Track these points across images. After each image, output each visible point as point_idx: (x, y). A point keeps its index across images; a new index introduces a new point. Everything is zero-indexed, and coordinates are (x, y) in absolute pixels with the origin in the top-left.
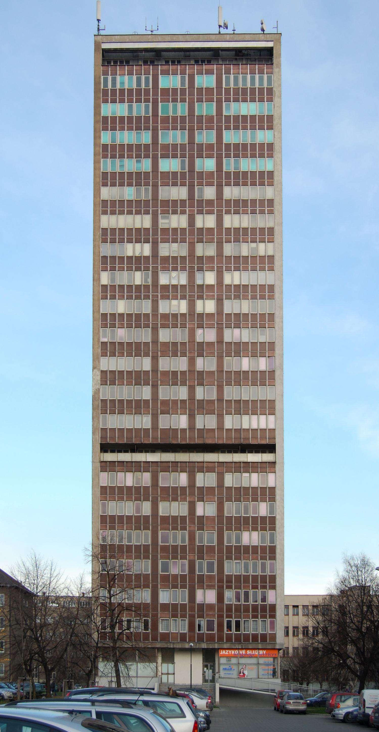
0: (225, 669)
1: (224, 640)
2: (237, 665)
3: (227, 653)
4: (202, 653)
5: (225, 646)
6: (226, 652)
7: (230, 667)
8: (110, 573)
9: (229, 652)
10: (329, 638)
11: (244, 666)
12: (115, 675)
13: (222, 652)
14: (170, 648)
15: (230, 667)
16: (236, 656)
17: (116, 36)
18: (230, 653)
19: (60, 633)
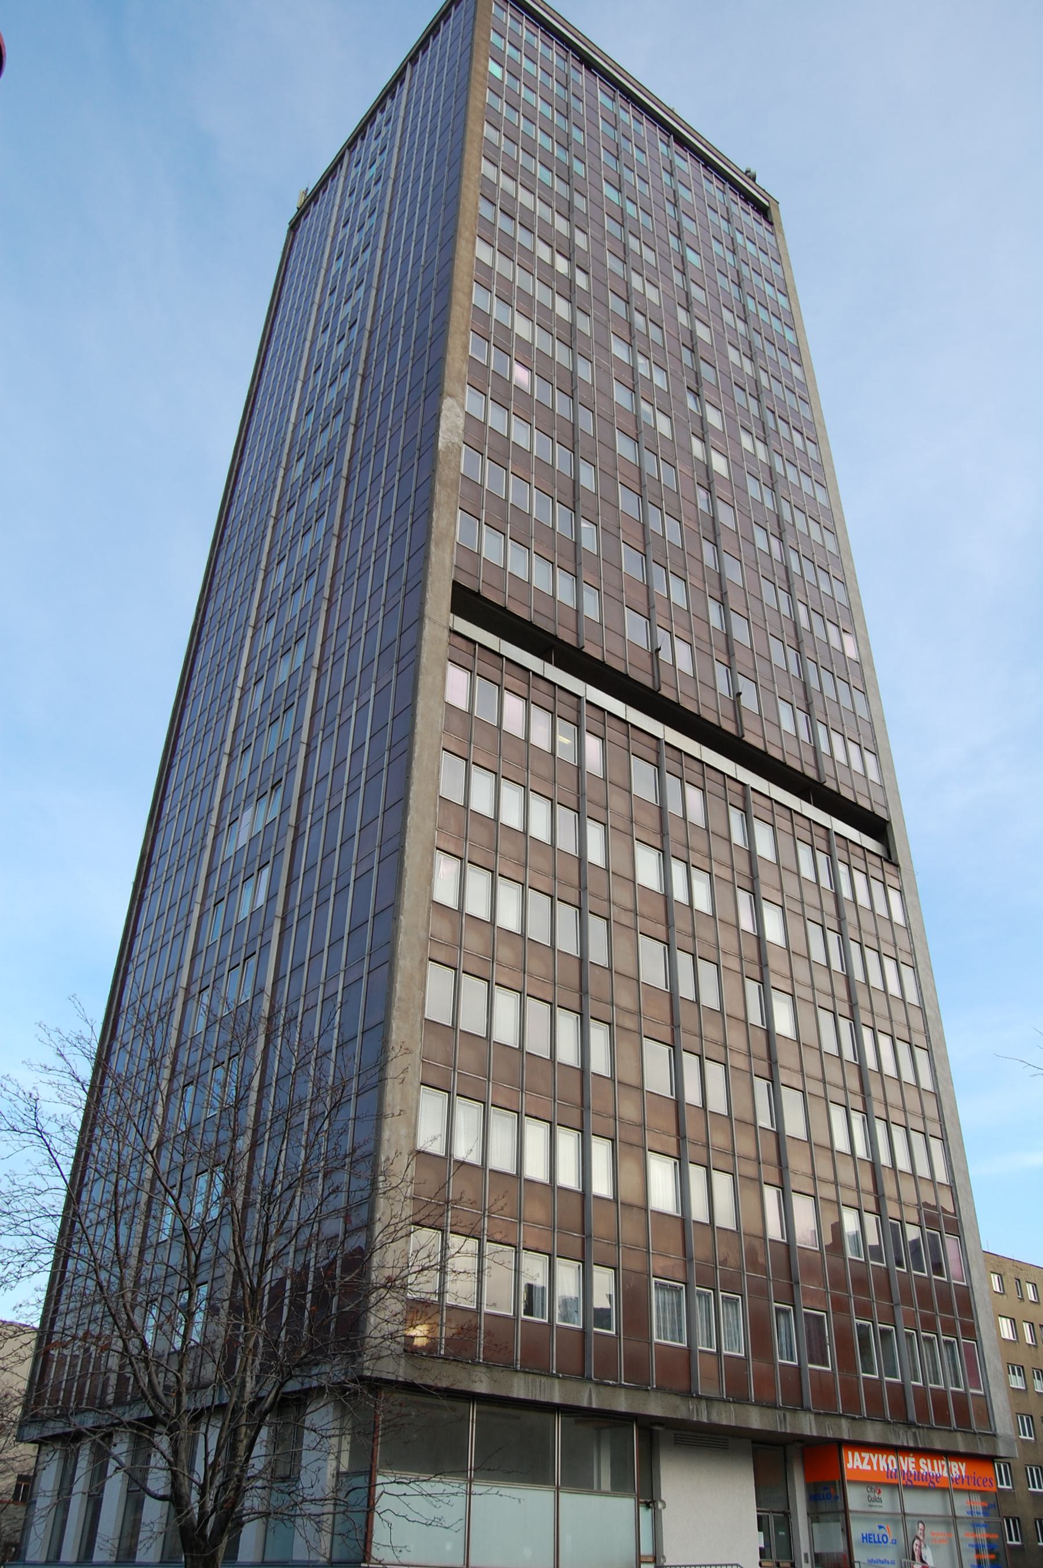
0: (867, 1538)
1: (860, 1406)
2: (947, 1524)
3: (866, 1467)
4: (751, 1459)
5: (872, 1433)
6: (862, 1459)
7: (882, 1531)
8: (465, 1419)
9: (870, 1463)
10: (196, 1483)
11: (921, 1525)
12: (374, 1376)
13: (855, 1462)
14: (700, 1424)
15: (882, 1531)
16: (893, 1481)
17: (453, 851)
18: (875, 1468)
19: (408, 1415)
